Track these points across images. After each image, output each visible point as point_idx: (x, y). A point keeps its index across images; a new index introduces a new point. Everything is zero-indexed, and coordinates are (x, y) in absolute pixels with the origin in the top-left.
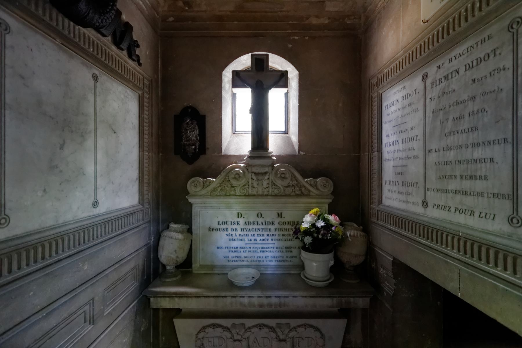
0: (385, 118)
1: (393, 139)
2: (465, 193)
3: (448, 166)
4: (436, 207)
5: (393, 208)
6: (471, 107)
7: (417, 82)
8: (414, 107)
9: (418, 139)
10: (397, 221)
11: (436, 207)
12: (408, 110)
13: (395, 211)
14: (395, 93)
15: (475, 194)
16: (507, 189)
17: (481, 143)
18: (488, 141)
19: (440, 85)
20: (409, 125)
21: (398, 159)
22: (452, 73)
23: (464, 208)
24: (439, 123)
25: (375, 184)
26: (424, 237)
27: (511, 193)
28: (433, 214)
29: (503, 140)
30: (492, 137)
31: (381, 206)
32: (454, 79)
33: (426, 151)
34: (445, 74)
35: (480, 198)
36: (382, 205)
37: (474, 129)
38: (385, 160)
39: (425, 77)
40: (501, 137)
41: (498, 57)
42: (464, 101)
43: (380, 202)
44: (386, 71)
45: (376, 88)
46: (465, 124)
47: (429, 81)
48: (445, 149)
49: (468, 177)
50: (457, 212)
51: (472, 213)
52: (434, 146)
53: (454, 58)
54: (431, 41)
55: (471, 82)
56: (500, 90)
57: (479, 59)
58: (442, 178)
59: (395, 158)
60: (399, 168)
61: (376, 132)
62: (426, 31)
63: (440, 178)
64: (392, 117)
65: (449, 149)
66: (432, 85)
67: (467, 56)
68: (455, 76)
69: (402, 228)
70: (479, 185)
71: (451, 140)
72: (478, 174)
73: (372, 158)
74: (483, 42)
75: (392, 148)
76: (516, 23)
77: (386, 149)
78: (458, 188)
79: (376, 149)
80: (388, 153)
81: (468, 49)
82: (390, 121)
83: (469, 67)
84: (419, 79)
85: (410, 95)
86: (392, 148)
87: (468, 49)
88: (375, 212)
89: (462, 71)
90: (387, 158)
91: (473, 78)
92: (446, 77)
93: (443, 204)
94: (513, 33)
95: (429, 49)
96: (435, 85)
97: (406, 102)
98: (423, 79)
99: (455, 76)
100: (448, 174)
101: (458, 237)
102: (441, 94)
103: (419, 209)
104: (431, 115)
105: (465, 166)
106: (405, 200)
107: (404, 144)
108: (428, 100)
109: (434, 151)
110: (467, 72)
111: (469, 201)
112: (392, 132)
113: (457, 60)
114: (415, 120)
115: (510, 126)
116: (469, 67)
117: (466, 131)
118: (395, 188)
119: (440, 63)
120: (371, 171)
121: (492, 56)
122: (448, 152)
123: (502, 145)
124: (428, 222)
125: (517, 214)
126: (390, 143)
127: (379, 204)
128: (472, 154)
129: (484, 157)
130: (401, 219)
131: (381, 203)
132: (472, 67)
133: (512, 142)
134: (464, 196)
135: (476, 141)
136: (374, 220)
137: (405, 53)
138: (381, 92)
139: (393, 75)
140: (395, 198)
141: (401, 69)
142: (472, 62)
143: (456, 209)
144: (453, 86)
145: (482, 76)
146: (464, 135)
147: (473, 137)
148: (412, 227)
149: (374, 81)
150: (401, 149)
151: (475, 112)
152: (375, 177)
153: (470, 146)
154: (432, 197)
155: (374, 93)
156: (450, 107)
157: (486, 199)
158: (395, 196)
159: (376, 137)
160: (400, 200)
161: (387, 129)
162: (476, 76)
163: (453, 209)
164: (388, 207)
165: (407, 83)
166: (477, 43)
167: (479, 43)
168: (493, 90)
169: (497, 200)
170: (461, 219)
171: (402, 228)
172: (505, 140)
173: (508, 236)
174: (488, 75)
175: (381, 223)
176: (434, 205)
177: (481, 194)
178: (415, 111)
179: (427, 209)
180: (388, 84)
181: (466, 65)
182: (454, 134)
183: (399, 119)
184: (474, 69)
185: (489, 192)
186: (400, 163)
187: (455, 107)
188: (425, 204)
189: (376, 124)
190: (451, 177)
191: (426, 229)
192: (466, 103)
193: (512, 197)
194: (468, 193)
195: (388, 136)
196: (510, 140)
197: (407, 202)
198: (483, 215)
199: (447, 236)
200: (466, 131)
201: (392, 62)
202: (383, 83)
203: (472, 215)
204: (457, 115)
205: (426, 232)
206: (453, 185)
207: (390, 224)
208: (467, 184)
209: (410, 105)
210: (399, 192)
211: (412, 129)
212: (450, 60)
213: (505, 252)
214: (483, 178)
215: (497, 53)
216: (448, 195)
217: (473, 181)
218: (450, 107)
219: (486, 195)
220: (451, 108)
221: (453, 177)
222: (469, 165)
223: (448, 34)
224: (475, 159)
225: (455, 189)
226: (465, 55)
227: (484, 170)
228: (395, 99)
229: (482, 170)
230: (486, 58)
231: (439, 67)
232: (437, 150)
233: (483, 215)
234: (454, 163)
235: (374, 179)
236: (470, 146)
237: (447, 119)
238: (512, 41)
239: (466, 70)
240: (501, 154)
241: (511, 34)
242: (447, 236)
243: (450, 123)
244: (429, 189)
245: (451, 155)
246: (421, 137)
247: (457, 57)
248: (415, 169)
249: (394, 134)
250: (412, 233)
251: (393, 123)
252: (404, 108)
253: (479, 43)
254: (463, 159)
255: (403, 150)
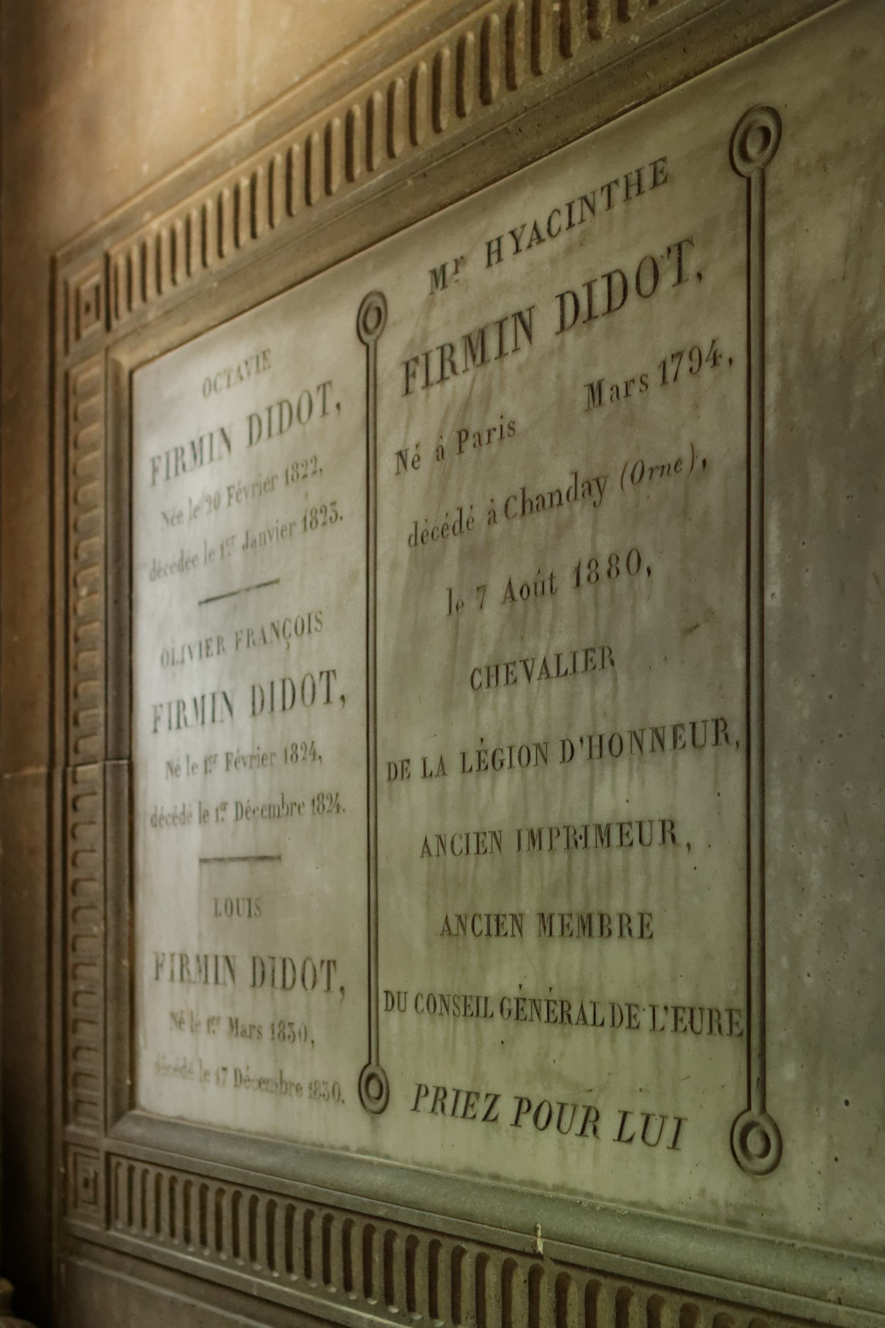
0: (152, 543)
1: (199, 679)
2: (561, 1013)
3: (484, 859)
4: (427, 1103)
5: (207, 1131)
6: (590, 534)
7: (329, 337)
8: (316, 492)
9: (336, 691)
10: (227, 1213)
11: (427, 1103)
12: (283, 507)
13: (216, 1148)
14: (210, 387)
15: (604, 1013)
16: (723, 988)
17: (626, 738)
18: (655, 731)
19: (449, 385)
20: (291, 605)
21: (231, 812)
22: (501, 324)
23: (558, 1094)
24: (442, 605)
25: (90, 976)
26: (368, 1291)
27: (741, 1004)
28: (418, 1144)
29: (711, 726)
30: (668, 710)
31: (127, 1127)
32: (511, 363)
33: (381, 772)
34: (469, 327)
35: (623, 1034)
36: (138, 1120)
37: (597, 657)
38: (157, 821)
39: (372, 319)
40: (704, 711)
41: (690, 287)
42: (556, 499)
43: (124, 1098)
44: (156, 226)
45: (93, 327)
46: (558, 631)
47: (392, 350)
48: (472, 760)
49: (574, 925)
50: (527, 1120)
51: (591, 1121)
52: (413, 739)
53: (508, 245)
54: (400, 108)
55: (583, 395)
56: (699, 464)
57: (617, 279)
58: (456, 928)
59: (212, 805)
60: (234, 869)
61: (97, 627)
62: (373, 40)
63: (447, 930)
64: (197, 535)
65: (488, 761)
66: (409, 375)
67: (569, 250)
68: (516, 349)
69: (253, 1256)
70: (617, 968)
71: (500, 715)
72: (616, 905)
73: (70, 805)
74: (634, 190)
75: (192, 742)
76: (759, 138)
77: (158, 748)
78: (531, 989)
79: (99, 740)
80: (173, 769)
81: (570, 206)
82: (184, 564)
83: (577, 313)
84: (342, 322)
85: (295, 415)
86: (192, 742)
87: (570, 206)
88: (95, 1168)
89: (546, 323)
90: (168, 806)
91: (595, 378)
92: (475, 345)
93: (464, 1083)
94: (749, 180)
95: (391, 153)
96: (420, 381)
97: (275, 453)
98: (362, 329)
99: (516, 349)
100: (484, 908)
101: (531, 1262)
102: (449, 441)
103: (341, 1126)
104: (405, 553)
105: (561, 858)
106: (268, 1072)
107: (263, 719)
108: (387, 463)
109: (416, 768)
110: (569, 336)
111: (580, 1054)
112: (192, 636)
113: (524, 255)
114: (322, 574)
115: (739, 662)
116: (577, 313)
117: (566, 664)
118: (211, 1001)
119: (444, 253)
120: (70, 889)
121: (669, 277)
122: (485, 780)
123: (709, 750)
124: (388, 1199)
125: (763, 1109)
126: (181, 704)
127: (118, 1115)
128: (591, 798)
129: (637, 814)
130: (247, 1195)
131: (132, 1105)
132: (590, 316)
133: (743, 743)
134: (556, 1029)
135: (604, 728)
136: (87, 1222)
137: (262, 138)
138: (126, 360)
139: (196, 261)
140: (212, 1063)
141: (244, 236)
142: (589, 286)
143: (523, 1104)
144: (511, 405)
145: (629, 376)
146: (558, 688)
147: (595, 704)
148: (307, 1239)
149: (85, 277)
150: (247, 750)
151: (604, 567)
152: (91, 932)
153: (581, 753)
154: (418, 1049)
155: (85, 356)
156: (492, 519)
157: (645, 1038)
158: (214, 1049)
159: (93, 658)
160: (240, 1079)
161: (164, 611)
162: (610, 369)
163: (506, 1108)
164: (175, 1125)
165: (275, 334)
166: (609, 187)
167: (619, 193)
168: (671, 459)
169: (688, 1041)
170: (542, 1159)
171: (253, 1256)
172: (720, 725)
173: (731, 1222)
174: (655, 378)
175: (130, 1238)
176: (421, 1091)
177: (624, 1016)
178: (320, 517)
179: (383, 1119)
180: (167, 314)
181: (562, 297)
182: (511, 682)
183: (237, 557)
184: (598, 324)
185: (660, 1002)
186: (241, 838)
187: (517, 522)
188: (374, 1089)
189: (97, 571)
190: (496, 926)
191: (378, 1240)
192: (565, 510)
193: (743, 1024)
194: (575, 1013)
195: (169, 660)
196: (736, 730)
197: (280, 1086)
198: (635, 1125)
199: (481, 1263)
200: (566, 664)
201: (193, 180)
202: (137, 303)
203: (589, 1130)
204: (525, 573)
205: (377, 1258)
206: (507, 970)
207: (187, 1238)
208: (570, 963)
209: (296, 474)
210: (233, 1024)
211: (306, 626)
212: (494, 254)
213: (721, 1309)
214: (636, 926)
215: (691, 266)
216: (487, 1027)
217: (596, 942)
218: (492, 519)
219: (645, 1018)
220: (498, 529)
221: (508, 923)
222: (579, 856)
223: (485, 97)
224: (604, 821)
225: (514, 992)
226: (562, 240)
227: (638, 883)
228: (211, 424)
229: (631, 881)
230: (647, 285)
231: (439, 277)
232: (432, 766)
233: (635, 1125)
234: (509, 842)
235: (84, 944)
236: (581, 753)
237: (482, 589)
238: (743, 220)
239: (563, 328)
240: (694, 790)
241: (744, 182)
242: (481, 1263)
243: (493, 615)
244: (394, 1000)
245: (500, 798)
246: (350, 682)
247: (524, 243)
248: (322, 875)
249: (205, 649)
250: (308, 1275)
251: (203, 580)
252: (263, 487)
253: (619, 193)
254: (554, 820)
255: (260, 759)
